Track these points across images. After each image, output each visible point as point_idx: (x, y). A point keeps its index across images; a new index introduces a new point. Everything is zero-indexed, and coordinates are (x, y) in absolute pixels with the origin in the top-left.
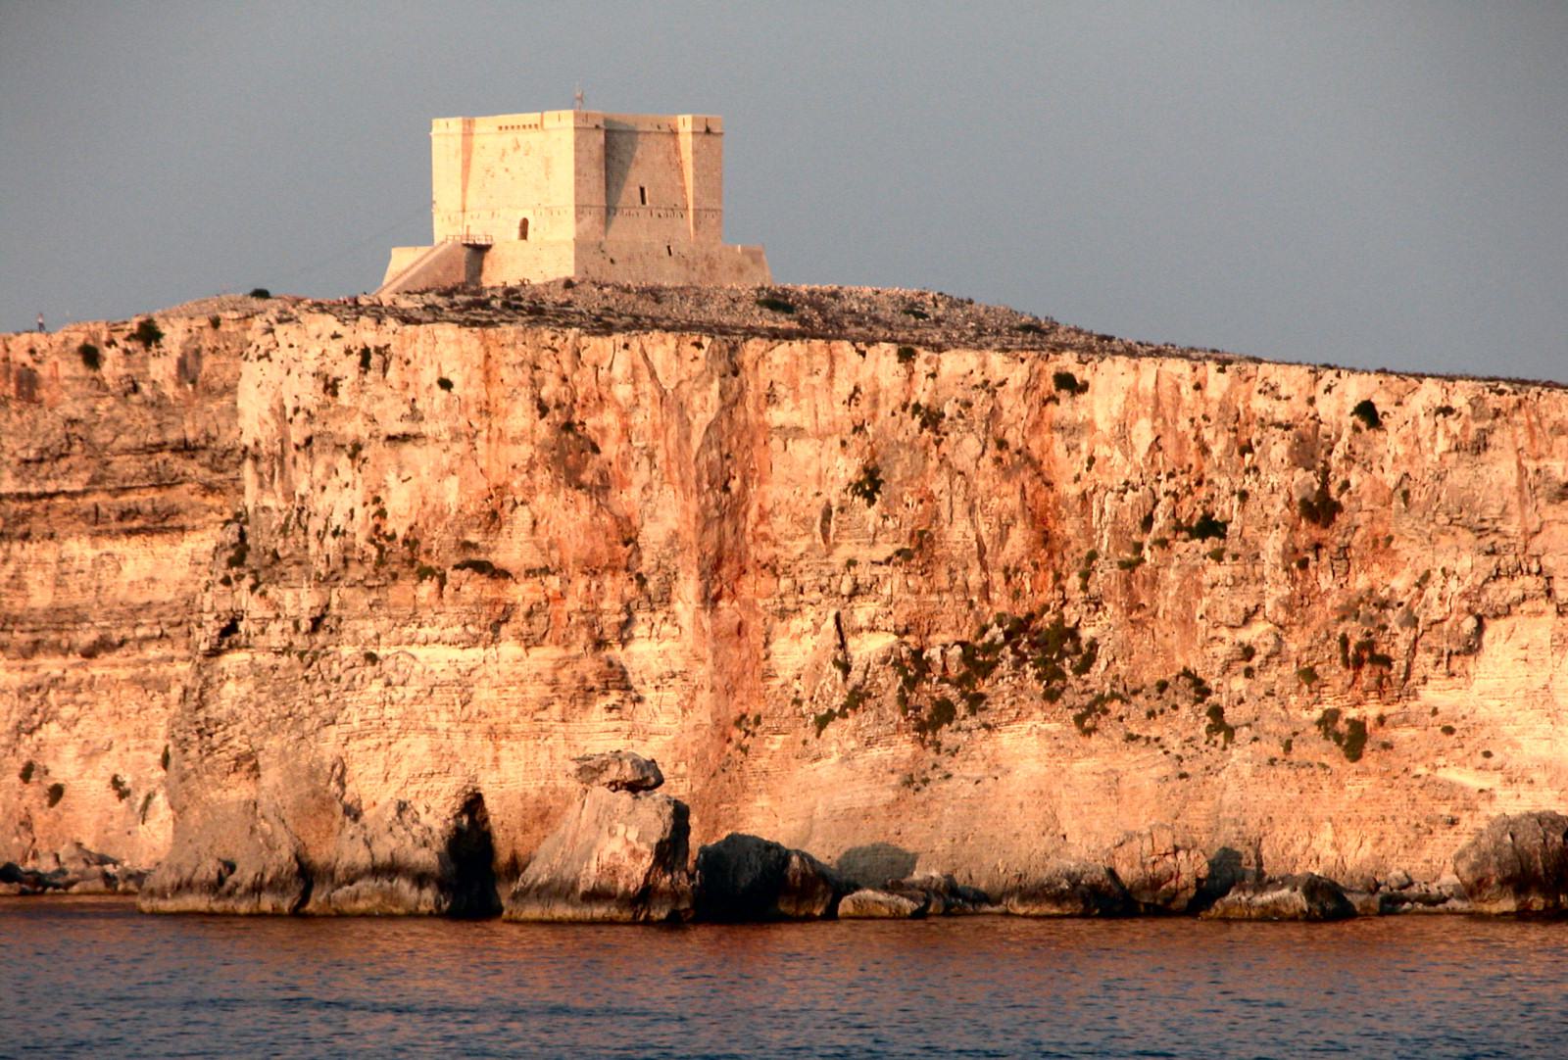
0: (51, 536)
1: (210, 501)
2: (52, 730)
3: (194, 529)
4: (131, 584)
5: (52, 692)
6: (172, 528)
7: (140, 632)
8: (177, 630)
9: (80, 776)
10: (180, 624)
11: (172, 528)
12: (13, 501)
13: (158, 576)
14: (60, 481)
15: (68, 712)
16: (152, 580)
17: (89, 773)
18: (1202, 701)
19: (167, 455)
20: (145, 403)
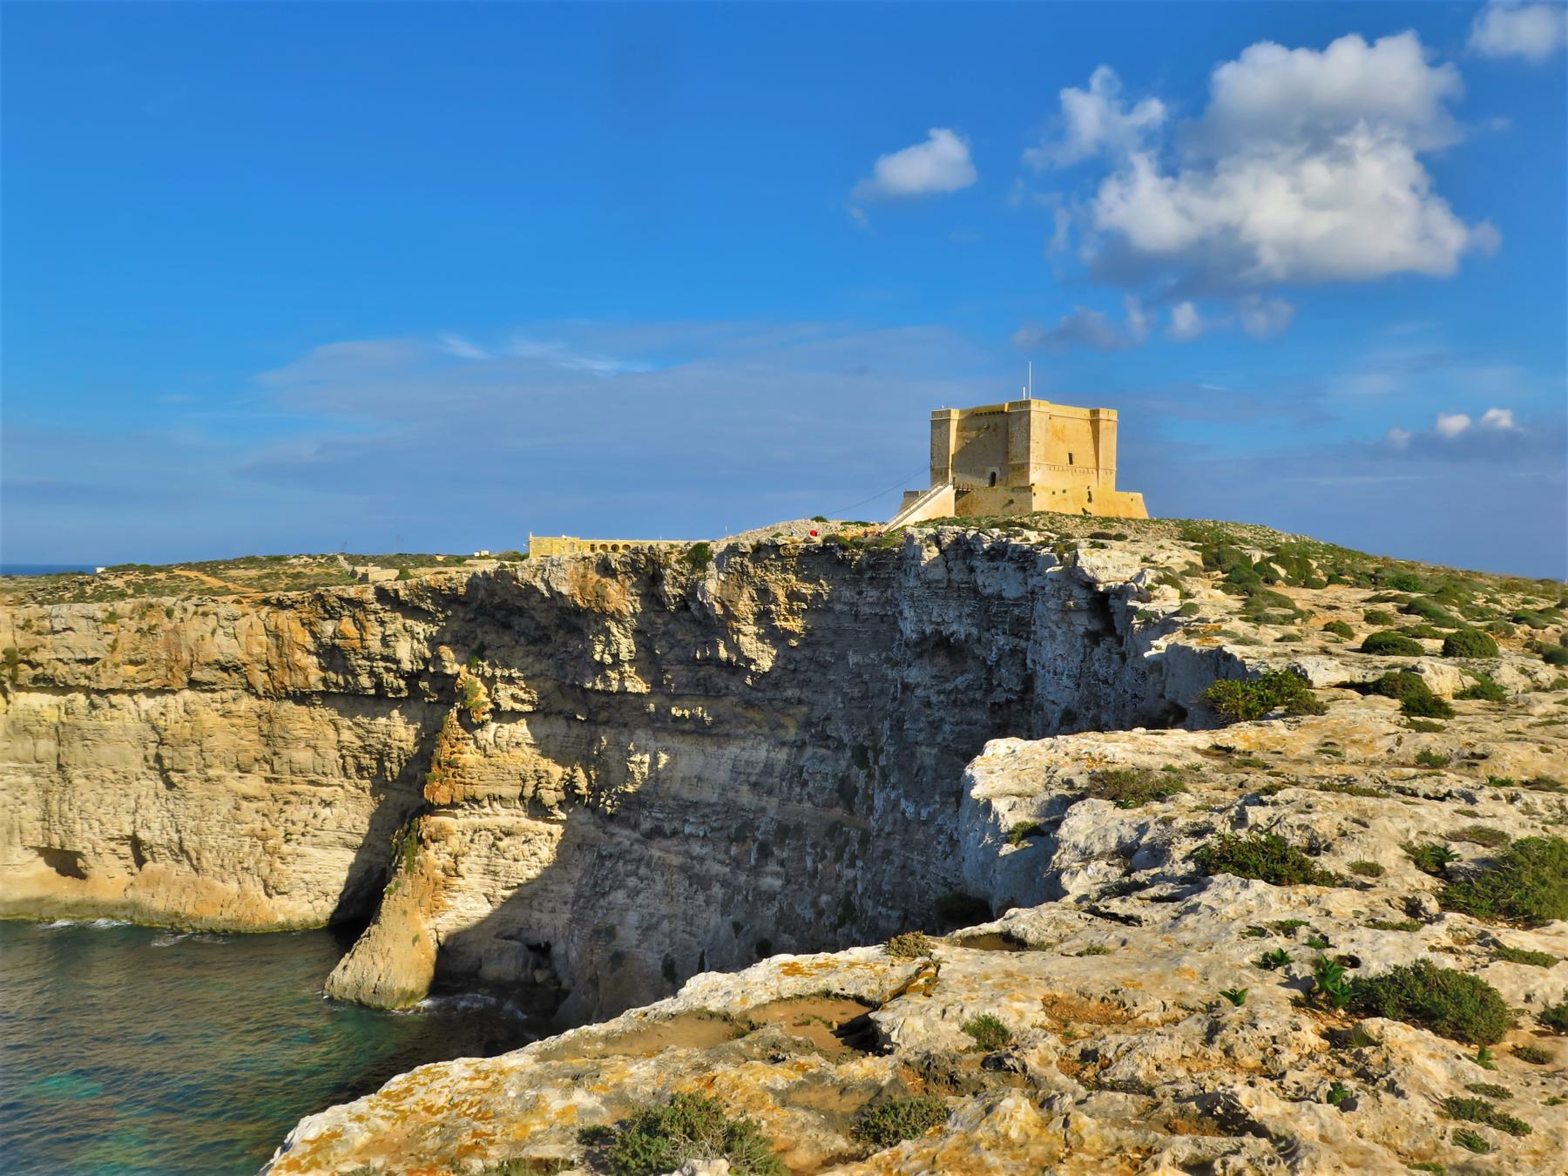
0: (625, 725)
1: (751, 714)
2: (619, 896)
3: (737, 737)
4: (683, 779)
5: (620, 864)
6: (717, 735)
7: (688, 829)
8: (718, 835)
9: (638, 946)
10: (721, 828)
11: (717, 735)
12: (1341, 877)
13: (706, 775)
14: (605, 1076)
15: (632, 882)
16: (700, 779)
17: (645, 945)
18: (1319, 947)
19: (713, 670)
20: (694, 620)
